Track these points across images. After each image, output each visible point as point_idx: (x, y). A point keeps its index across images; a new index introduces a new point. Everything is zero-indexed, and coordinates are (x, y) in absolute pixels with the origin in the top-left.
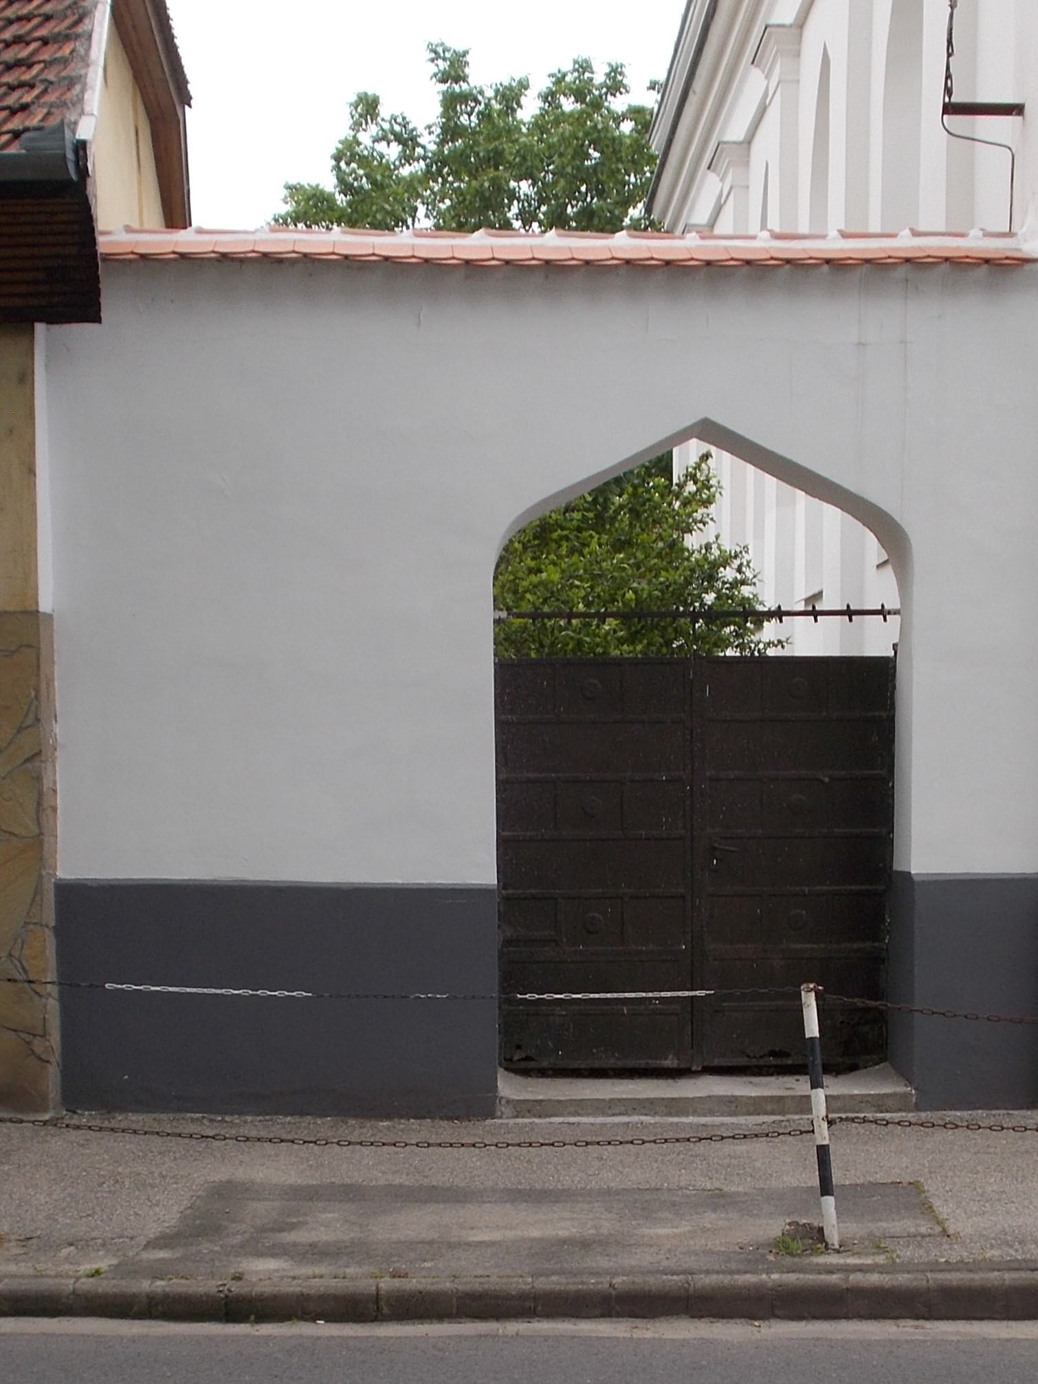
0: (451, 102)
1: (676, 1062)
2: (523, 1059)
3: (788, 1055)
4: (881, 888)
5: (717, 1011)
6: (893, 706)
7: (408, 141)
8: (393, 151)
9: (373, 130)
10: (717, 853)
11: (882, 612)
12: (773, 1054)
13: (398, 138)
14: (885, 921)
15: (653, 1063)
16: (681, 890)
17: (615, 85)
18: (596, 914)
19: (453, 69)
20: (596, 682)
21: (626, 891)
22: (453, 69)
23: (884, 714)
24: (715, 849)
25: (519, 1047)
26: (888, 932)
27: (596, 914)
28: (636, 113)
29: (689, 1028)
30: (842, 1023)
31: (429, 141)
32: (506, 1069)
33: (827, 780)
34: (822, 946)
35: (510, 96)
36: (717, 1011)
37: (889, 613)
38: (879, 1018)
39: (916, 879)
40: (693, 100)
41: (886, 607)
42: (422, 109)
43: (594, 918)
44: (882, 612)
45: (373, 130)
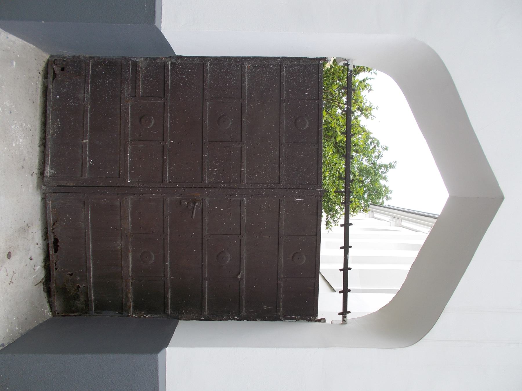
0: (386, 166)
1: (49, 175)
2: (54, 72)
3: (56, 251)
4: (169, 311)
5: (84, 204)
6: (286, 319)
7: (378, 157)
8: (376, 154)
9: (381, 150)
10: (192, 205)
11: (345, 312)
12: (56, 241)
13: (379, 155)
14: (147, 314)
15: (49, 159)
16: (167, 180)
17: (388, 198)
18: (153, 122)
19: (391, 166)
20: (307, 126)
21: (168, 144)
22: (391, 166)
23: (280, 313)
24: (195, 203)
25: (63, 69)
26: (139, 317)
27: (153, 122)
28: (383, 202)
29: (71, 184)
30: (79, 287)
31: (378, 162)
32: (48, 61)
33: (239, 277)
34: (131, 274)
35: (385, 178)
36: (84, 204)
37: (344, 317)
38: (85, 310)
39: (160, 355)
40: (406, 214)
41: (348, 315)
42: (384, 160)
43: (150, 122)
44: (345, 312)
45: (381, 150)
